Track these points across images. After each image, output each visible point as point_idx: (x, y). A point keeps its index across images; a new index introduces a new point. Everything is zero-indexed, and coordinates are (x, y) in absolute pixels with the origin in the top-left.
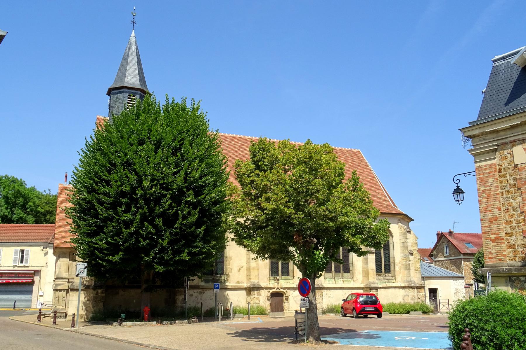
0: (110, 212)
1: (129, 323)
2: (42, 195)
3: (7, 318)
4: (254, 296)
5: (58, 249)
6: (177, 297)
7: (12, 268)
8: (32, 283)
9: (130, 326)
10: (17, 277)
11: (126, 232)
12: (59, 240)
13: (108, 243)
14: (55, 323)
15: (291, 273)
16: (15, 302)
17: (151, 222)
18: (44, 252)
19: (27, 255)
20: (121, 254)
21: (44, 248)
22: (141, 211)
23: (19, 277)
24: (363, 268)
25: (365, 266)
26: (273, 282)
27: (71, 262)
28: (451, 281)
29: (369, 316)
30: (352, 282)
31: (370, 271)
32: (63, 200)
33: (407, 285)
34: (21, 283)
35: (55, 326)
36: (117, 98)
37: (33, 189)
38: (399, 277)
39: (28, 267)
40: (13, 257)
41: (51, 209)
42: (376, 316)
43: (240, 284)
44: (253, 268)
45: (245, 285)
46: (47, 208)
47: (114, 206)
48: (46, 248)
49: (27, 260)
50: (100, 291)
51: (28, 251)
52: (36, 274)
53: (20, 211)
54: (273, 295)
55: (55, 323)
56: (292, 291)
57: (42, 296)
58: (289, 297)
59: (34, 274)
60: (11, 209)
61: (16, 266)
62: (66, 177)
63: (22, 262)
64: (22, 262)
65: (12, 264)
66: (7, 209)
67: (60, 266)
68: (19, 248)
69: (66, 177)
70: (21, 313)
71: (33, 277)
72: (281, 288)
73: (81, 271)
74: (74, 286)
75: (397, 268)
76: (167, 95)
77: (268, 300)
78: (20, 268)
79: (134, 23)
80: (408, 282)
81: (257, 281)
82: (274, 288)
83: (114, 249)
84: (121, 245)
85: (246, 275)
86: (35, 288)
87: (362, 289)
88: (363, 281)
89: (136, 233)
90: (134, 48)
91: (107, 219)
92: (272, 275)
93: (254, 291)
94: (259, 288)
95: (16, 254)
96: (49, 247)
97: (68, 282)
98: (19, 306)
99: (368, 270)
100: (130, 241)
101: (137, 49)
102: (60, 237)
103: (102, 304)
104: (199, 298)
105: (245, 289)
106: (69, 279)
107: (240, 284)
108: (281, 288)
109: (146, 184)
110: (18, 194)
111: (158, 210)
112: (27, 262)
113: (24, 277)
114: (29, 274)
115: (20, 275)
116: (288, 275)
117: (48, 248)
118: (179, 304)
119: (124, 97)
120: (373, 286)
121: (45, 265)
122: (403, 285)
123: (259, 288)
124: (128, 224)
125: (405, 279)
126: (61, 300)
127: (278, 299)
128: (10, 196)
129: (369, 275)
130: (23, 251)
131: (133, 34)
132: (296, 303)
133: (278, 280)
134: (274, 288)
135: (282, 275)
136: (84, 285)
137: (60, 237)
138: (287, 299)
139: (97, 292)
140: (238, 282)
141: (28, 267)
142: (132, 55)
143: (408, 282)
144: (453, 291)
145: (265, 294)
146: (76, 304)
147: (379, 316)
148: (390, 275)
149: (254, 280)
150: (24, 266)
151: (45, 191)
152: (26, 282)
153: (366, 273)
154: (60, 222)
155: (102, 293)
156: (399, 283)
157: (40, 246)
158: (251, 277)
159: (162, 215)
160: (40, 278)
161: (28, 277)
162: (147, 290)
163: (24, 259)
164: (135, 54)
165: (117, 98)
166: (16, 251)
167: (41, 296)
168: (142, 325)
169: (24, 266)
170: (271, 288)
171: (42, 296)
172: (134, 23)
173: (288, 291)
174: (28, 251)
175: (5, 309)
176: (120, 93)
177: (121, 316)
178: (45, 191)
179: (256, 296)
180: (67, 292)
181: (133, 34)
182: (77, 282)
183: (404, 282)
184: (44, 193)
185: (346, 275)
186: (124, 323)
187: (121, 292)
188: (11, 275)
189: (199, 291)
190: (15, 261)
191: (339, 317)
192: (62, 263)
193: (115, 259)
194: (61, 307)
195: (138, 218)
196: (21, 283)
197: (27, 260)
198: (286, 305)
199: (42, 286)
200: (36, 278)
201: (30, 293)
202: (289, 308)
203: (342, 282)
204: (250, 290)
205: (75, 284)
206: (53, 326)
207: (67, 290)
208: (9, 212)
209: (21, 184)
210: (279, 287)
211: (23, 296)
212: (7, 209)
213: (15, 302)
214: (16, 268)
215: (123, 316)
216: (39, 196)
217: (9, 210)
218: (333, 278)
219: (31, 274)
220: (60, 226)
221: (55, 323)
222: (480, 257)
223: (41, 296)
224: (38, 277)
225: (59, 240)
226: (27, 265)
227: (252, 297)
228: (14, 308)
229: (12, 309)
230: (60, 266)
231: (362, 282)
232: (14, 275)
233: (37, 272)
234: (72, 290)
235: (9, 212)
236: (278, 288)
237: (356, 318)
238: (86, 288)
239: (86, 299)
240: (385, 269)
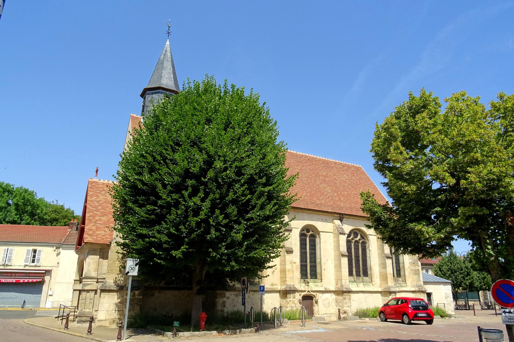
0: (175, 196)
1: (187, 334)
2: (50, 205)
3: (15, 321)
4: (290, 299)
5: (88, 245)
6: (217, 300)
7: (22, 268)
8: (42, 283)
9: (187, 337)
10: (27, 276)
11: (193, 221)
12: (90, 235)
13: (170, 235)
14: (67, 327)
15: (318, 276)
16: (24, 302)
17: (223, 210)
18: (56, 252)
19: (39, 255)
20: (183, 248)
21: (56, 248)
22: (211, 196)
23: (29, 276)
24: (380, 273)
25: (383, 270)
26: (303, 285)
27: (101, 260)
28: (442, 286)
29: (412, 322)
30: (371, 285)
31: (388, 275)
32: (93, 195)
33: (417, 289)
34: (32, 282)
35: (91, 337)
36: (152, 98)
37: (41, 200)
38: (409, 281)
39: (40, 266)
40: (25, 256)
41: (57, 217)
42: (424, 322)
43: (274, 287)
44: (289, 271)
45: (279, 288)
46: (53, 216)
47: (178, 188)
48: (59, 248)
49: (39, 260)
50: (137, 292)
51: (40, 251)
52: (47, 273)
53: (27, 217)
54: (305, 298)
55: (67, 327)
56: (321, 295)
57: (52, 295)
58: (319, 301)
59: (45, 273)
60: (20, 215)
61: (27, 265)
62: (97, 171)
63: (33, 261)
64: (33, 261)
65: (23, 263)
66: (16, 215)
67: (89, 264)
68: (31, 248)
69: (97, 171)
70: (32, 314)
71: (44, 276)
72: (312, 291)
73: (132, 269)
74: (106, 286)
75: (407, 273)
76: (226, 80)
77: (300, 303)
78: (31, 267)
79: (169, 33)
80: (418, 286)
81: (292, 284)
82: (305, 291)
83: (177, 241)
84: (184, 237)
85: (279, 277)
86: (45, 287)
87: (413, 292)
88: (381, 284)
89: (206, 221)
90: (169, 54)
91: (168, 206)
92: (302, 278)
93: (290, 293)
94: (294, 291)
95: (28, 254)
96: (62, 247)
97: (97, 282)
98: (28, 306)
99: (386, 274)
100: (197, 231)
101: (172, 56)
102: (91, 232)
103: (138, 307)
104: (236, 301)
105: (279, 292)
106: (98, 279)
107: (274, 287)
108: (312, 291)
109: (218, 164)
110: (27, 202)
111: (231, 196)
112: (38, 262)
113: (34, 276)
114: (39, 273)
115: (30, 275)
116: (316, 278)
117: (61, 249)
118: (219, 308)
119: (159, 98)
120: (392, 290)
121: (56, 265)
122: (413, 289)
123: (294, 291)
124: (196, 212)
125: (415, 283)
126: (88, 302)
127: (308, 302)
128: (20, 203)
129: (388, 279)
130: (35, 251)
131: (168, 43)
132: (325, 306)
133: (308, 283)
134: (305, 291)
135: (311, 278)
136: (118, 286)
137: (91, 232)
138: (317, 302)
139: (134, 294)
140: (272, 285)
141: (40, 266)
142: (168, 61)
143: (418, 286)
144: (444, 295)
145: (298, 296)
146: (107, 309)
147: (429, 321)
148: (400, 279)
149: (289, 282)
150: (35, 266)
151: (53, 202)
152: (37, 282)
153: (384, 277)
154: (90, 216)
155: (139, 294)
156: (409, 287)
157: (53, 246)
158: (287, 279)
159: (234, 202)
160: (51, 277)
161: (39, 276)
162: (199, 293)
163: (36, 259)
164: (170, 60)
165: (152, 98)
166: (28, 251)
167: (50, 295)
168: (202, 336)
169: (35, 266)
170: (302, 291)
171: (52, 295)
172: (169, 33)
173: (318, 294)
174: (40, 251)
175: (14, 309)
176: (156, 93)
177: (173, 324)
178: (53, 202)
179: (292, 299)
180: (96, 294)
181: (168, 43)
182: (110, 282)
183: (414, 286)
184: (52, 203)
185: (366, 278)
186: (181, 334)
187: (157, 293)
188: (21, 275)
189: (235, 293)
190: (26, 261)
191: (377, 323)
192: (91, 261)
193: (177, 254)
194: (87, 310)
195: (208, 203)
196: (32, 282)
197: (39, 260)
198: (315, 308)
199: (52, 286)
200: (47, 278)
201: (40, 292)
202: (318, 312)
203: (363, 286)
204: (285, 293)
205: (107, 284)
206: (87, 336)
207: (96, 291)
208: (18, 218)
209: (32, 194)
210: (310, 290)
211: (31, 295)
212: (16, 215)
213: (24, 302)
214: (27, 268)
215: (176, 324)
216: (47, 205)
217: (18, 216)
218: (355, 281)
219: (42, 273)
220: (90, 220)
221: (67, 327)
222: (441, 266)
223: (50, 295)
224: (49, 277)
225: (90, 235)
226: (38, 265)
227: (288, 300)
228: (23, 307)
229: (20, 309)
230: (89, 264)
231: (380, 287)
232: (24, 275)
233: (48, 272)
234: (103, 291)
235: (18, 218)
236: (309, 291)
237: (407, 324)
238: (121, 289)
239: (119, 300)
240: (356, 274)
